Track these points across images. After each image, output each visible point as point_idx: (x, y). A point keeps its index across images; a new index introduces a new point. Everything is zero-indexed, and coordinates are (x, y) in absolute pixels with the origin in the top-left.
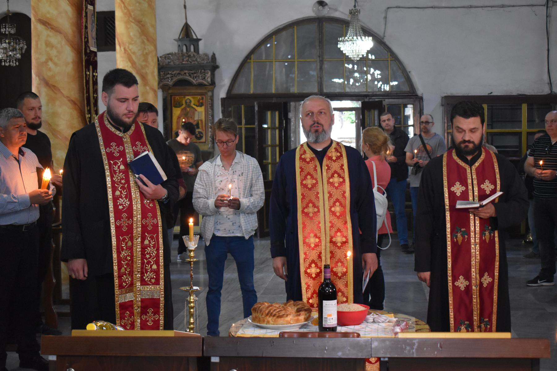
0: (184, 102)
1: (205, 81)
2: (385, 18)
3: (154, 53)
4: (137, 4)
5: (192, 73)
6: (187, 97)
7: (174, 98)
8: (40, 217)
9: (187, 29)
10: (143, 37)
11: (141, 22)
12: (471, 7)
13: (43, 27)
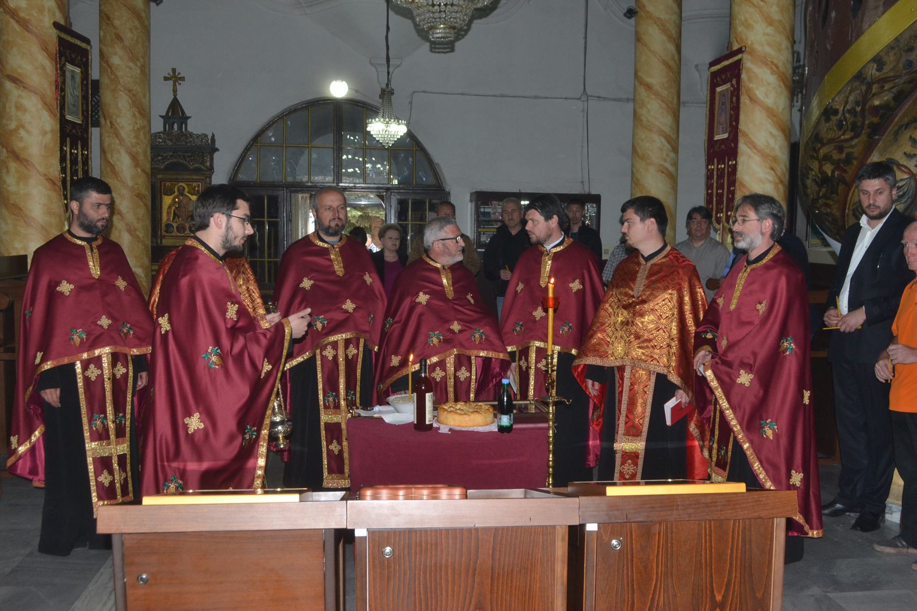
0: (176, 190)
1: (203, 165)
2: (411, 103)
3: (147, 129)
4: (128, 70)
5: (188, 156)
6: (180, 184)
7: (165, 184)
8: (707, 345)
9: (175, 105)
10: (134, 109)
11: (132, 91)
12: (502, 96)
13: (13, 85)
